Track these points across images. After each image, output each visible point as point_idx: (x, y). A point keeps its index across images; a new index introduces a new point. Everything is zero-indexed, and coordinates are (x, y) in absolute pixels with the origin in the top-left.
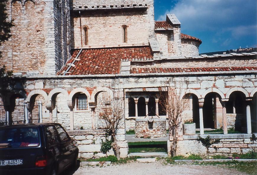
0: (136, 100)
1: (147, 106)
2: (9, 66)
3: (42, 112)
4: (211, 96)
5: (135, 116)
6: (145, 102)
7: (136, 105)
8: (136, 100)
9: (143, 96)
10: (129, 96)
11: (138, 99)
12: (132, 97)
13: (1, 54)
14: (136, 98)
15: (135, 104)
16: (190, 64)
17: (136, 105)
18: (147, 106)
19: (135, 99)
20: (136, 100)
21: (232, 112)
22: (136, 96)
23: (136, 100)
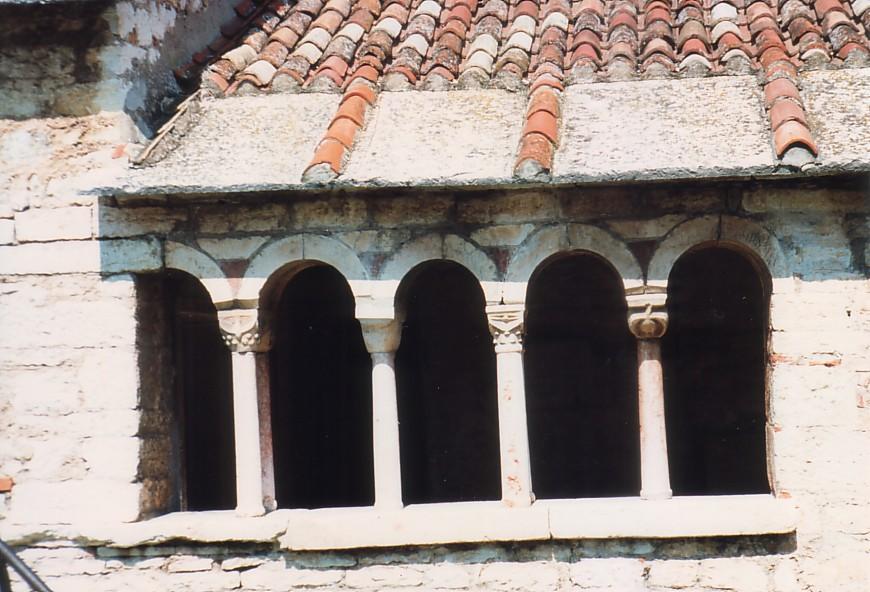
0: (237, 299)
1: (650, 376)
2: (349, 247)
3: (57, 548)
4: (419, 79)
5: (359, 492)
6: (356, 326)
7: (384, 382)
8: (236, 305)
9: (323, 251)
10: (145, 258)
11: (251, 287)
12: (183, 259)
13: (88, 57)
14: (235, 269)
15: (219, 353)
16: (507, 78)
17: (384, 382)
18: (650, 376)
19: (219, 288)
20: (236, 305)
21: (152, 240)
22: (234, 250)
23: (237, 299)
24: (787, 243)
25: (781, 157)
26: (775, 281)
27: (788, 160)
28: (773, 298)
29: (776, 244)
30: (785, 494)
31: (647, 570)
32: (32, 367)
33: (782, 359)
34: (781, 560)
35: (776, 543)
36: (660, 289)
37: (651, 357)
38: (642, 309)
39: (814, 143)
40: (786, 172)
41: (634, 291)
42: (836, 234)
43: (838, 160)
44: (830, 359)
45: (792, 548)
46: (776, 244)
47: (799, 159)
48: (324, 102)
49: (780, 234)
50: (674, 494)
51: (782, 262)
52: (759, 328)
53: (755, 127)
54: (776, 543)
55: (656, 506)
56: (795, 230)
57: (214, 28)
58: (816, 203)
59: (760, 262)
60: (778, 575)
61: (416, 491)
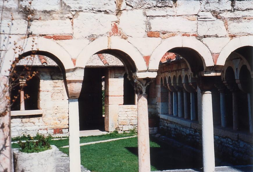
5: (18, 109)
24: (42, 75)
25: (42, 64)
26: (41, 80)
27: (43, 64)
28: (83, 76)
29: (41, 75)
30: (41, 109)
31: (22, 120)
32: (241, 35)
33: (41, 91)
34: (41, 118)
35: (40, 116)
36: (25, 81)
37: (22, 91)
38: (22, 84)
39: (46, 62)
40: (43, 66)
41: (21, 81)
42: (49, 74)
43: (50, 65)
44: (48, 91)
45: (42, 116)
46: (41, 75)
47: (45, 64)
48: (24, 40)
49: (41, 74)
50: (25, 110)
51: (42, 78)
52: (38, 87)
53: (38, 59)
54: (40, 116)
55: (23, 111)
56: (44, 74)
57: (57, 2)
58: (46, 70)
59: (38, 77)
60: (40, 120)
61: (27, 108)
